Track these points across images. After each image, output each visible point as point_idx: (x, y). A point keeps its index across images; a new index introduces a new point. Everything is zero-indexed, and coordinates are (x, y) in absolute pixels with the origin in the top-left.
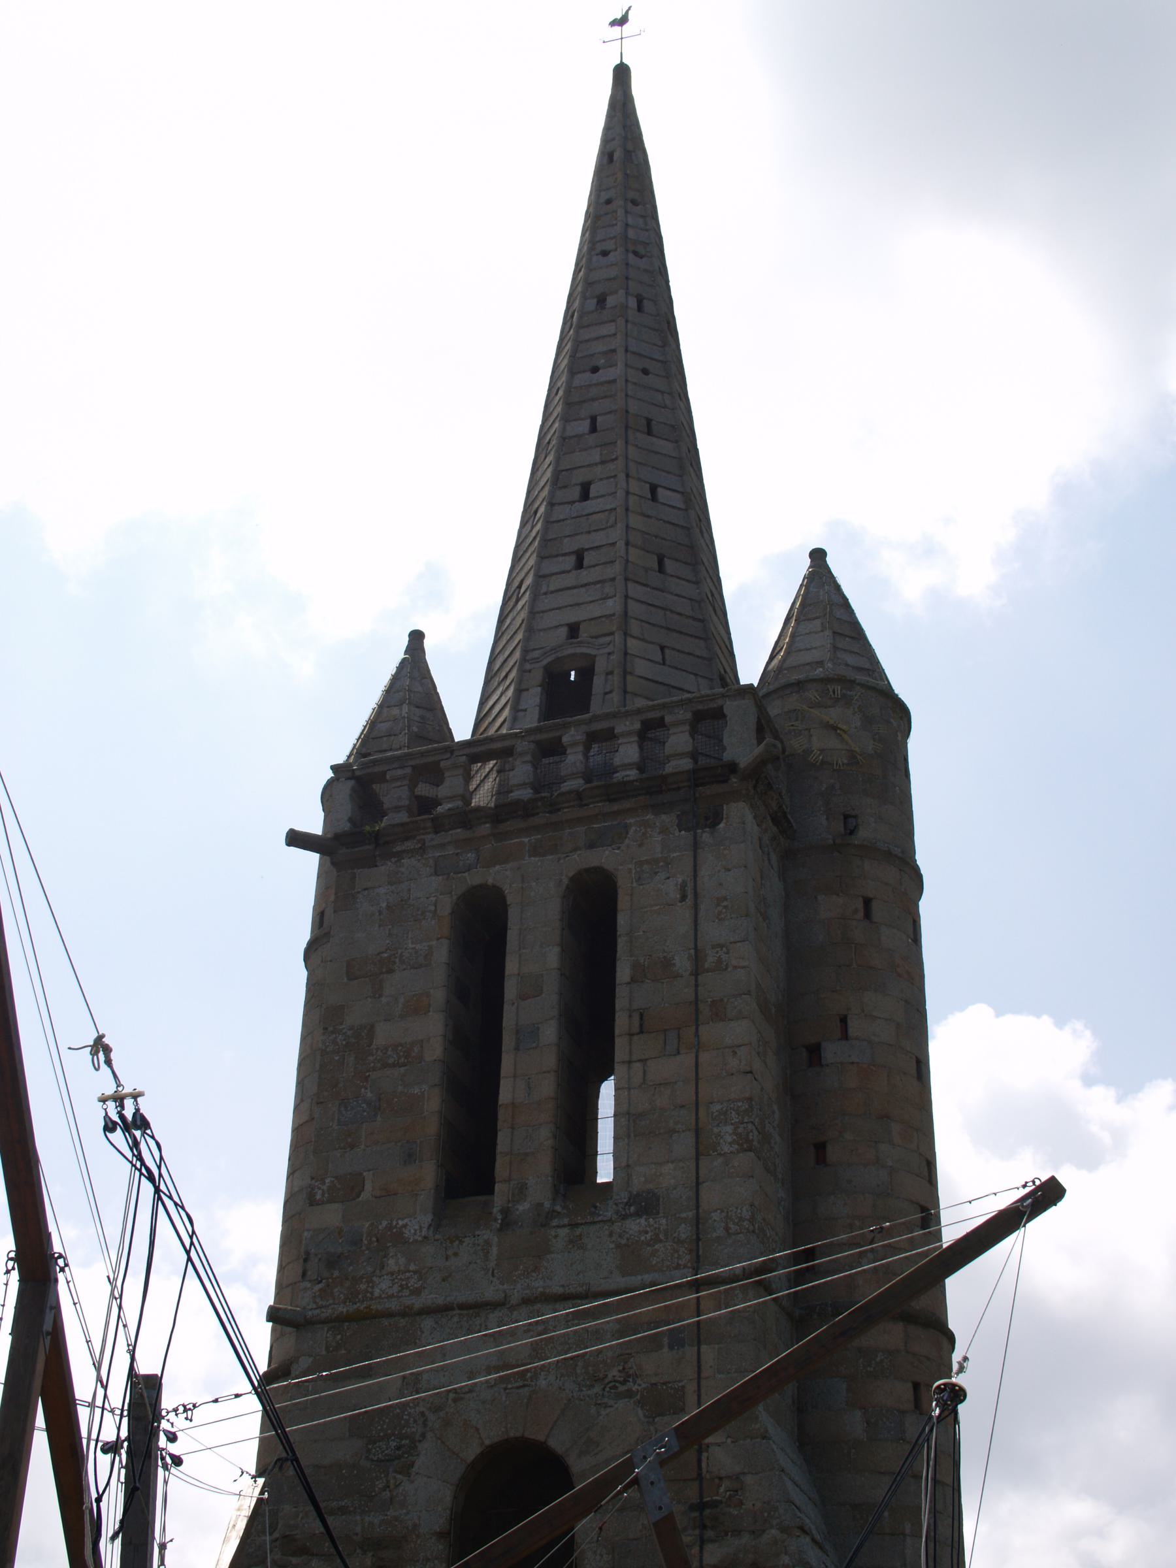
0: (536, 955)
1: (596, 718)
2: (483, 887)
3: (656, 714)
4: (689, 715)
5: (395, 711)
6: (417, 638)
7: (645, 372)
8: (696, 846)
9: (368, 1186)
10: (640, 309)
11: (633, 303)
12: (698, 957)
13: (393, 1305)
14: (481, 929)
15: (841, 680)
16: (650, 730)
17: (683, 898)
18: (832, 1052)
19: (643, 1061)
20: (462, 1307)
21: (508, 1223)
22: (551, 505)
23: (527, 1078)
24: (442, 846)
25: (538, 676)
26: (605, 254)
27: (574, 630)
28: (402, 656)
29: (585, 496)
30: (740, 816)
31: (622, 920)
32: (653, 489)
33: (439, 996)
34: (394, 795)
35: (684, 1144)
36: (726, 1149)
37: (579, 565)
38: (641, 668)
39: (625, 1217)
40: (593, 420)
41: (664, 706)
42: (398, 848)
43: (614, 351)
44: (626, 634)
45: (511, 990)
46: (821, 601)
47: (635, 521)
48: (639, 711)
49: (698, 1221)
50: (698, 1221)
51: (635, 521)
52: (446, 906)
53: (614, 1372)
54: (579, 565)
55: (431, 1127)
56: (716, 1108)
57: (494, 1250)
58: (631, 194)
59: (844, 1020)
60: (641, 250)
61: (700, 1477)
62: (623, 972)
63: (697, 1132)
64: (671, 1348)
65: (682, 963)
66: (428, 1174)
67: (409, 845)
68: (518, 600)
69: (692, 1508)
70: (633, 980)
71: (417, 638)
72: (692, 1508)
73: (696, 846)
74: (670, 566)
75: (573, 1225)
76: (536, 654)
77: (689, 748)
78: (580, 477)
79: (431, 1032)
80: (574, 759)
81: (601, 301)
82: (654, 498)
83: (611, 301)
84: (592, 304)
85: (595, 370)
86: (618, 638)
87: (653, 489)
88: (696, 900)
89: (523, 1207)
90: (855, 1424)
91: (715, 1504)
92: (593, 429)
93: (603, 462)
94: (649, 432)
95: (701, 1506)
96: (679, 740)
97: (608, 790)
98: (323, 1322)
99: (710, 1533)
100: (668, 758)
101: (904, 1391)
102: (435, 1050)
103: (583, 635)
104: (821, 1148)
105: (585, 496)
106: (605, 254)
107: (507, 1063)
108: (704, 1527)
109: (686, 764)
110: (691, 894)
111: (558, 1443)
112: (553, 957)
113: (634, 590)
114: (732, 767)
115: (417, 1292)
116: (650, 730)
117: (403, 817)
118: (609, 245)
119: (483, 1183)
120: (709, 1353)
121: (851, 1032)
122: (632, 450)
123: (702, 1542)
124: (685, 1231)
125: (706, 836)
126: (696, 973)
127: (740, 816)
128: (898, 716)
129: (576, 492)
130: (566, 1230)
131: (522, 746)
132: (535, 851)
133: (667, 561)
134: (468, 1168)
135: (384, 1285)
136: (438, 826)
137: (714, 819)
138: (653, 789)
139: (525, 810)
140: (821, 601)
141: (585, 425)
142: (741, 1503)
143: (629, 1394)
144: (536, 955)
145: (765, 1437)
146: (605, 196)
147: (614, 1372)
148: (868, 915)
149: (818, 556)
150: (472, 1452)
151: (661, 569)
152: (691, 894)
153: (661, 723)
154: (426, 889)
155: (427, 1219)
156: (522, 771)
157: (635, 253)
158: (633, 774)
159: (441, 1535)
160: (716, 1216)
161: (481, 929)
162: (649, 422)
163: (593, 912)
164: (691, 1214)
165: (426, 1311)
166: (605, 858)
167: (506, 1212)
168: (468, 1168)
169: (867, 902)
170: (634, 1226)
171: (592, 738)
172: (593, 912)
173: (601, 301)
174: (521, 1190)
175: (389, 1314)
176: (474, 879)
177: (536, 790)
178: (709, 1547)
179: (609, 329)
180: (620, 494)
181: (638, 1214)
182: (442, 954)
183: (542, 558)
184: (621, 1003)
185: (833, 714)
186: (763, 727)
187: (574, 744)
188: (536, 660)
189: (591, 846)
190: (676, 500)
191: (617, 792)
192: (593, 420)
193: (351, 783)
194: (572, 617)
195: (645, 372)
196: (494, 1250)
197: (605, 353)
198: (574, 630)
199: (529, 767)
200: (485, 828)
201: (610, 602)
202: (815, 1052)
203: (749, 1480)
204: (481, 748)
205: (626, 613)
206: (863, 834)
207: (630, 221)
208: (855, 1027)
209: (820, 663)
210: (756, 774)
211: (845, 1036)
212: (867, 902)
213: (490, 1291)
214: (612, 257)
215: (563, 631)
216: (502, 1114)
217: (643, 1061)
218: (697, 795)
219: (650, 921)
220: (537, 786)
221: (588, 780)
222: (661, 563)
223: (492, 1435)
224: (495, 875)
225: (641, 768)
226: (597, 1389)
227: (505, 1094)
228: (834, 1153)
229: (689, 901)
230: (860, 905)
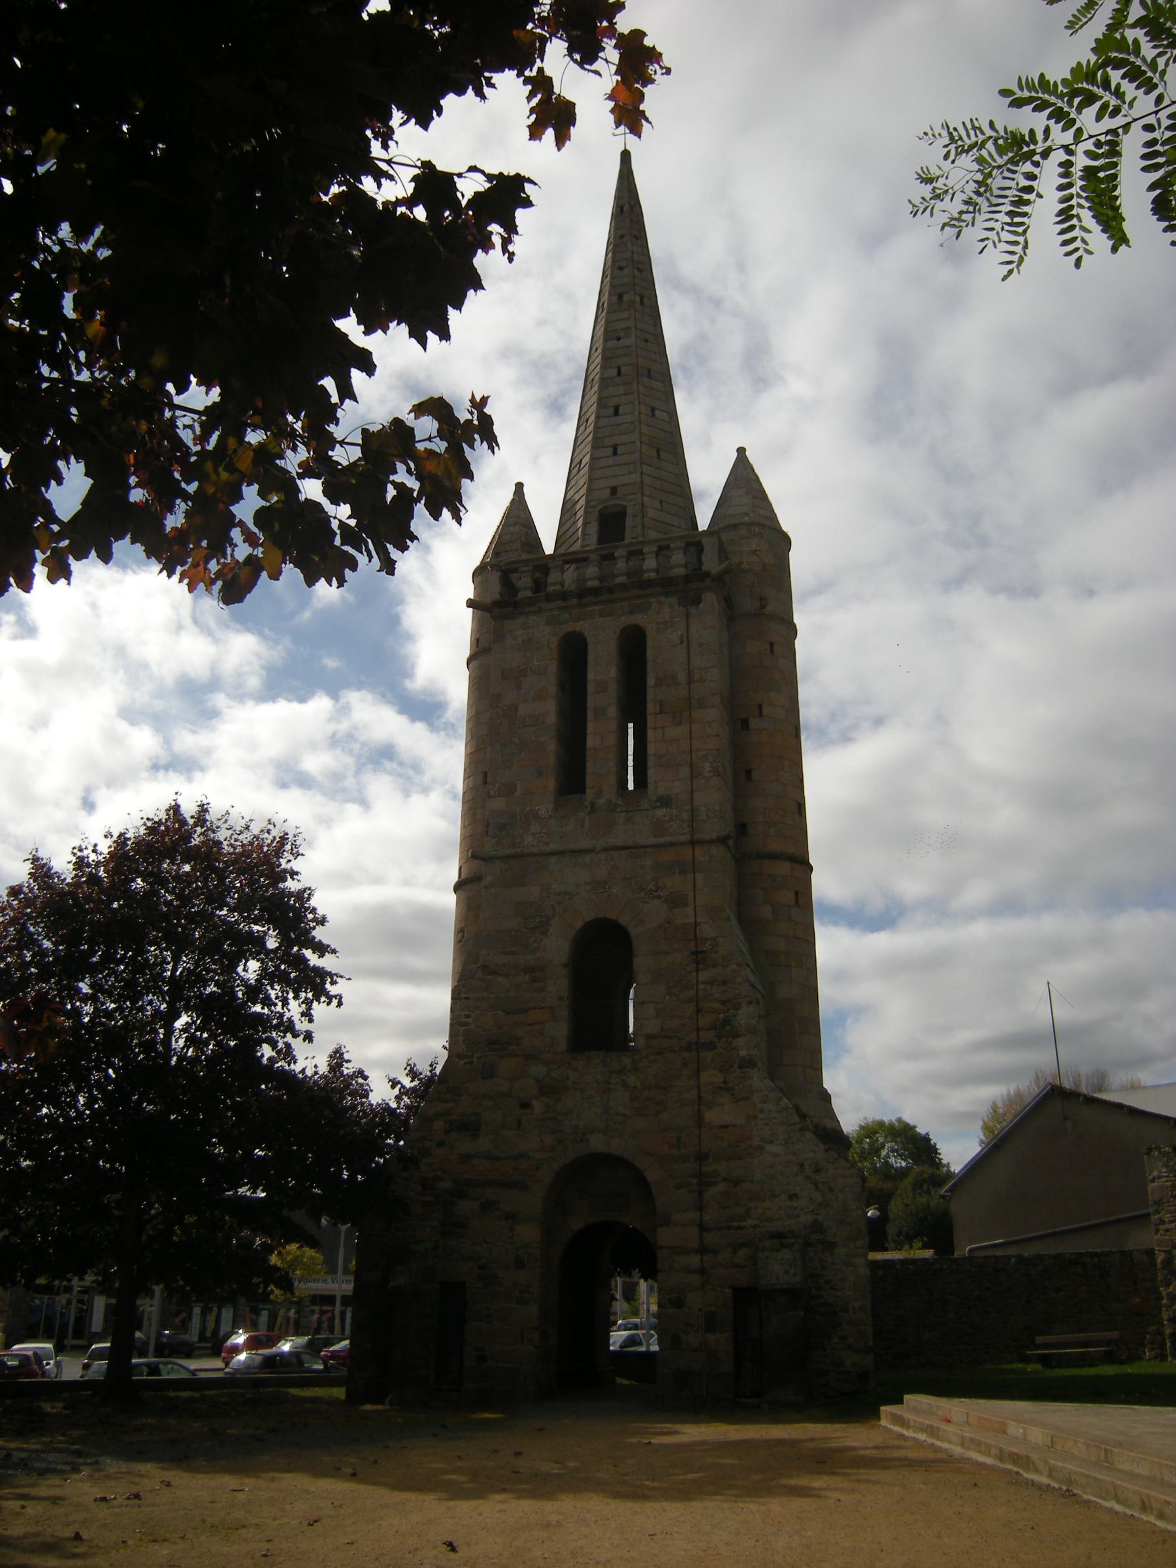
0: (603, 670)
1: (630, 544)
2: (574, 633)
3: (666, 543)
4: (683, 544)
5: (512, 529)
6: (519, 487)
7: (646, 341)
8: (688, 616)
9: (519, 788)
10: (642, 303)
11: (638, 299)
12: (690, 675)
13: (535, 850)
14: (574, 655)
15: (759, 524)
16: (663, 549)
17: (682, 643)
18: (754, 723)
19: (663, 728)
20: (572, 852)
21: (593, 809)
22: (598, 417)
23: (597, 735)
24: (551, 610)
25: (595, 515)
26: (621, 268)
27: (614, 491)
28: (511, 497)
29: (616, 413)
30: (710, 600)
31: (650, 653)
32: (653, 410)
33: (553, 689)
34: (524, 581)
35: (685, 772)
36: (707, 774)
37: (615, 453)
38: (651, 513)
39: (654, 808)
40: (619, 369)
41: (669, 539)
42: (527, 610)
43: (629, 328)
44: (643, 494)
45: (591, 688)
46: (743, 478)
47: (645, 429)
48: (656, 541)
49: (693, 812)
50: (693, 812)
51: (645, 429)
52: (554, 642)
53: (651, 886)
54: (615, 453)
55: (552, 760)
56: (701, 753)
57: (587, 824)
58: (635, 233)
59: (760, 707)
60: (641, 267)
61: (696, 938)
62: (651, 681)
63: (691, 765)
64: (680, 874)
65: (682, 677)
66: (551, 783)
67: (534, 608)
68: (579, 470)
69: (692, 953)
70: (656, 685)
71: (519, 487)
72: (692, 953)
73: (688, 616)
74: (662, 454)
75: (628, 812)
76: (593, 503)
77: (683, 562)
78: (614, 402)
79: (549, 710)
80: (621, 565)
81: (620, 297)
82: (653, 415)
83: (626, 298)
84: (615, 298)
85: (619, 339)
86: (639, 496)
87: (653, 410)
88: (686, 644)
89: (602, 801)
90: (767, 912)
91: (703, 952)
92: (619, 374)
93: (626, 394)
94: (650, 377)
95: (696, 953)
96: (678, 558)
97: (641, 585)
98: (499, 858)
99: (701, 966)
100: (672, 568)
101: (792, 896)
102: (552, 718)
103: (619, 494)
104: (749, 772)
105: (616, 413)
106: (621, 268)
107: (591, 726)
108: (698, 963)
109: (682, 571)
110: (686, 641)
111: (624, 920)
112: (613, 672)
113: (646, 469)
114: (708, 574)
115: (546, 844)
116: (663, 549)
117: (529, 593)
118: (623, 264)
119: (581, 789)
120: (700, 878)
121: (765, 712)
122: (641, 388)
123: (698, 970)
124: (685, 816)
125: (693, 610)
126: (689, 683)
127: (710, 600)
128: (784, 541)
129: (611, 411)
130: (623, 814)
131: (593, 557)
132: (602, 614)
133: (661, 452)
134: (572, 778)
135: (529, 839)
136: (549, 598)
137: (697, 601)
138: (666, 584)
139: (595, 592)
140: (743, 478)
141: (615, 371)
142: (717, 952)
143: (659, 897)
144: (603, 670)
145: (728, 919)
146: (619, 233)
147: (651, 886)
148: (772, 651)
149: (741, 451)
150: (579, 924)
151: (659, 457)
152: (686, 641)
153: (668, 547)
154: (542, 633)
155: (551, 806)
156: (592, 571)
157: (639, 269)
158: (653, 575)
159: (566, 965)
160: (702, 808)
161: (574, 655)
162: (649, 370)
163: (633, 647)
164: (688, 807)
165: (552, 854)
166: (638, 619)
167: (592, 804)
168: (572, 778)
169: (772, 645)
170: (660, 812)
171: (631, 554)
172: (633, 647)
173: (620, 297)
174: (600, 793)
175: (533, 855)
176: (570, 627)
177: (601, 582)
178: (700, 973)
179: (625, 315)
180: (636, 413)
181: (661, 806)
182: (553, 667)
183: (594, 448)
184: (649, 697)
185: (754, 544)
186: (723, 554)
187: (621, 557)
188: (594, 507)
189: (631, 613)
190: (665, 416)
191: (644, 585)
192: (619, 369)
193: (499, 574)
194: (612, 482)
195: (646, 341)
196: (587, 824)
197: (624, 329)
198: (614, 491)
199: (596, 569)
200: (574, 601)
201: (633, 476)
202: (745, 723)
203: (721, 940)
204: (564, 555)
205: (642, 482)
206: (769, 609)
207: (634, 249)
208: (766, 710)
209: (746, 514)
210: (719, 578)
211: (761, 715)
212: (772, 645)
213: (585, 844)
214: (626, 271)
215: (607, 492)
216: (588, 753)
217: (663, 728)
218: (688, 587)
219: (665, 652)
220: (602, 579)
221: (629, 577)
222: (658, 451)
223: (589, 916)
224: (579, 626)
225: (657, 571)
226: (643, 894)
227: (590, 743)
228: (755, 775)
229: (685, 644)
230: (768, 646)
